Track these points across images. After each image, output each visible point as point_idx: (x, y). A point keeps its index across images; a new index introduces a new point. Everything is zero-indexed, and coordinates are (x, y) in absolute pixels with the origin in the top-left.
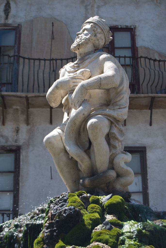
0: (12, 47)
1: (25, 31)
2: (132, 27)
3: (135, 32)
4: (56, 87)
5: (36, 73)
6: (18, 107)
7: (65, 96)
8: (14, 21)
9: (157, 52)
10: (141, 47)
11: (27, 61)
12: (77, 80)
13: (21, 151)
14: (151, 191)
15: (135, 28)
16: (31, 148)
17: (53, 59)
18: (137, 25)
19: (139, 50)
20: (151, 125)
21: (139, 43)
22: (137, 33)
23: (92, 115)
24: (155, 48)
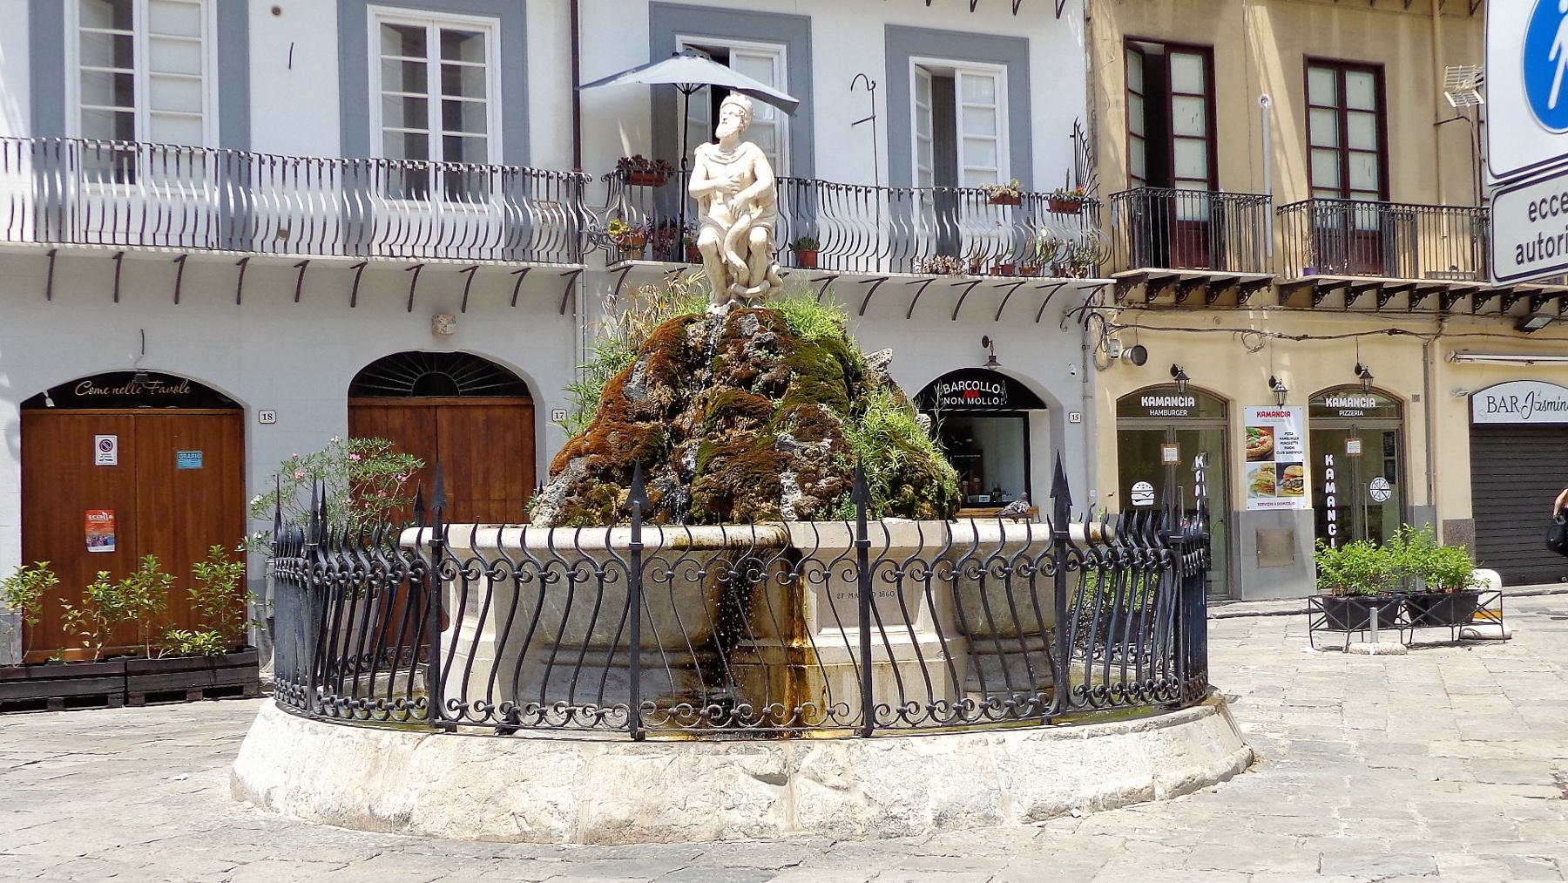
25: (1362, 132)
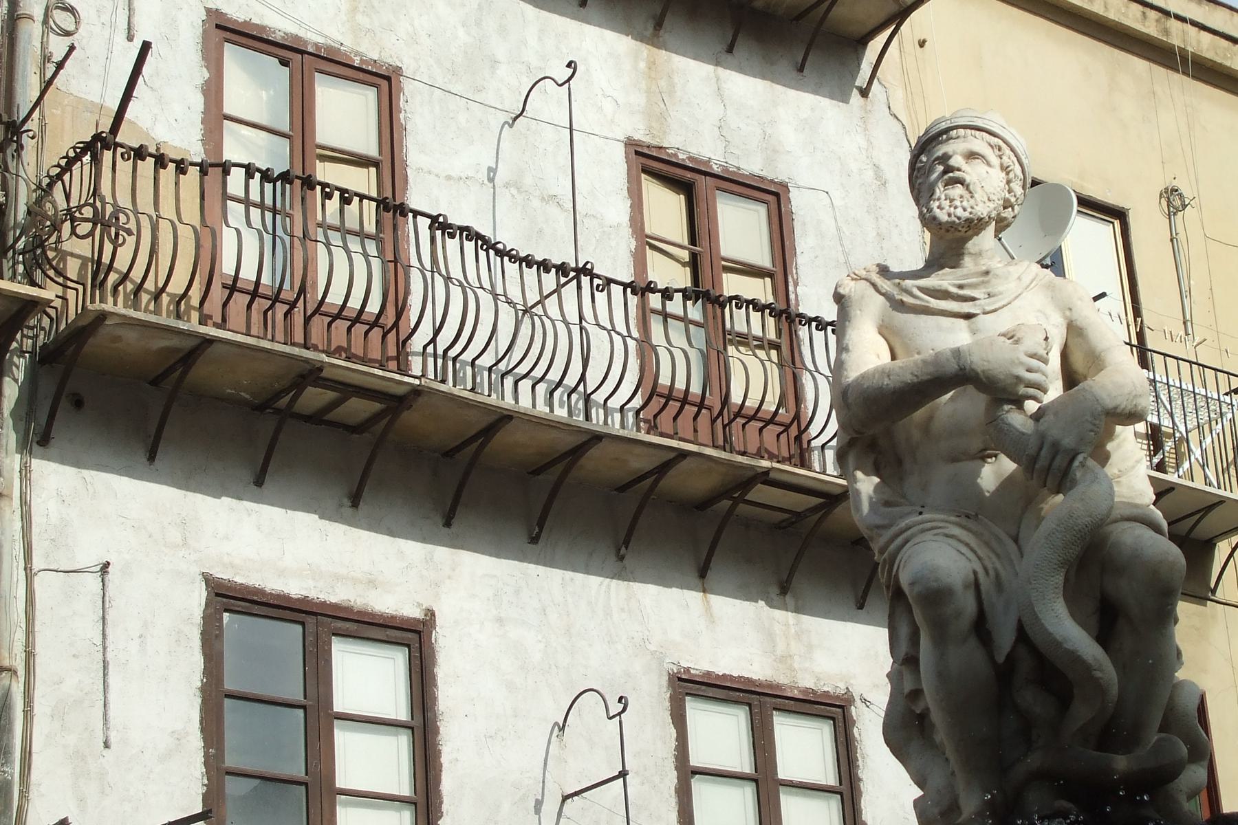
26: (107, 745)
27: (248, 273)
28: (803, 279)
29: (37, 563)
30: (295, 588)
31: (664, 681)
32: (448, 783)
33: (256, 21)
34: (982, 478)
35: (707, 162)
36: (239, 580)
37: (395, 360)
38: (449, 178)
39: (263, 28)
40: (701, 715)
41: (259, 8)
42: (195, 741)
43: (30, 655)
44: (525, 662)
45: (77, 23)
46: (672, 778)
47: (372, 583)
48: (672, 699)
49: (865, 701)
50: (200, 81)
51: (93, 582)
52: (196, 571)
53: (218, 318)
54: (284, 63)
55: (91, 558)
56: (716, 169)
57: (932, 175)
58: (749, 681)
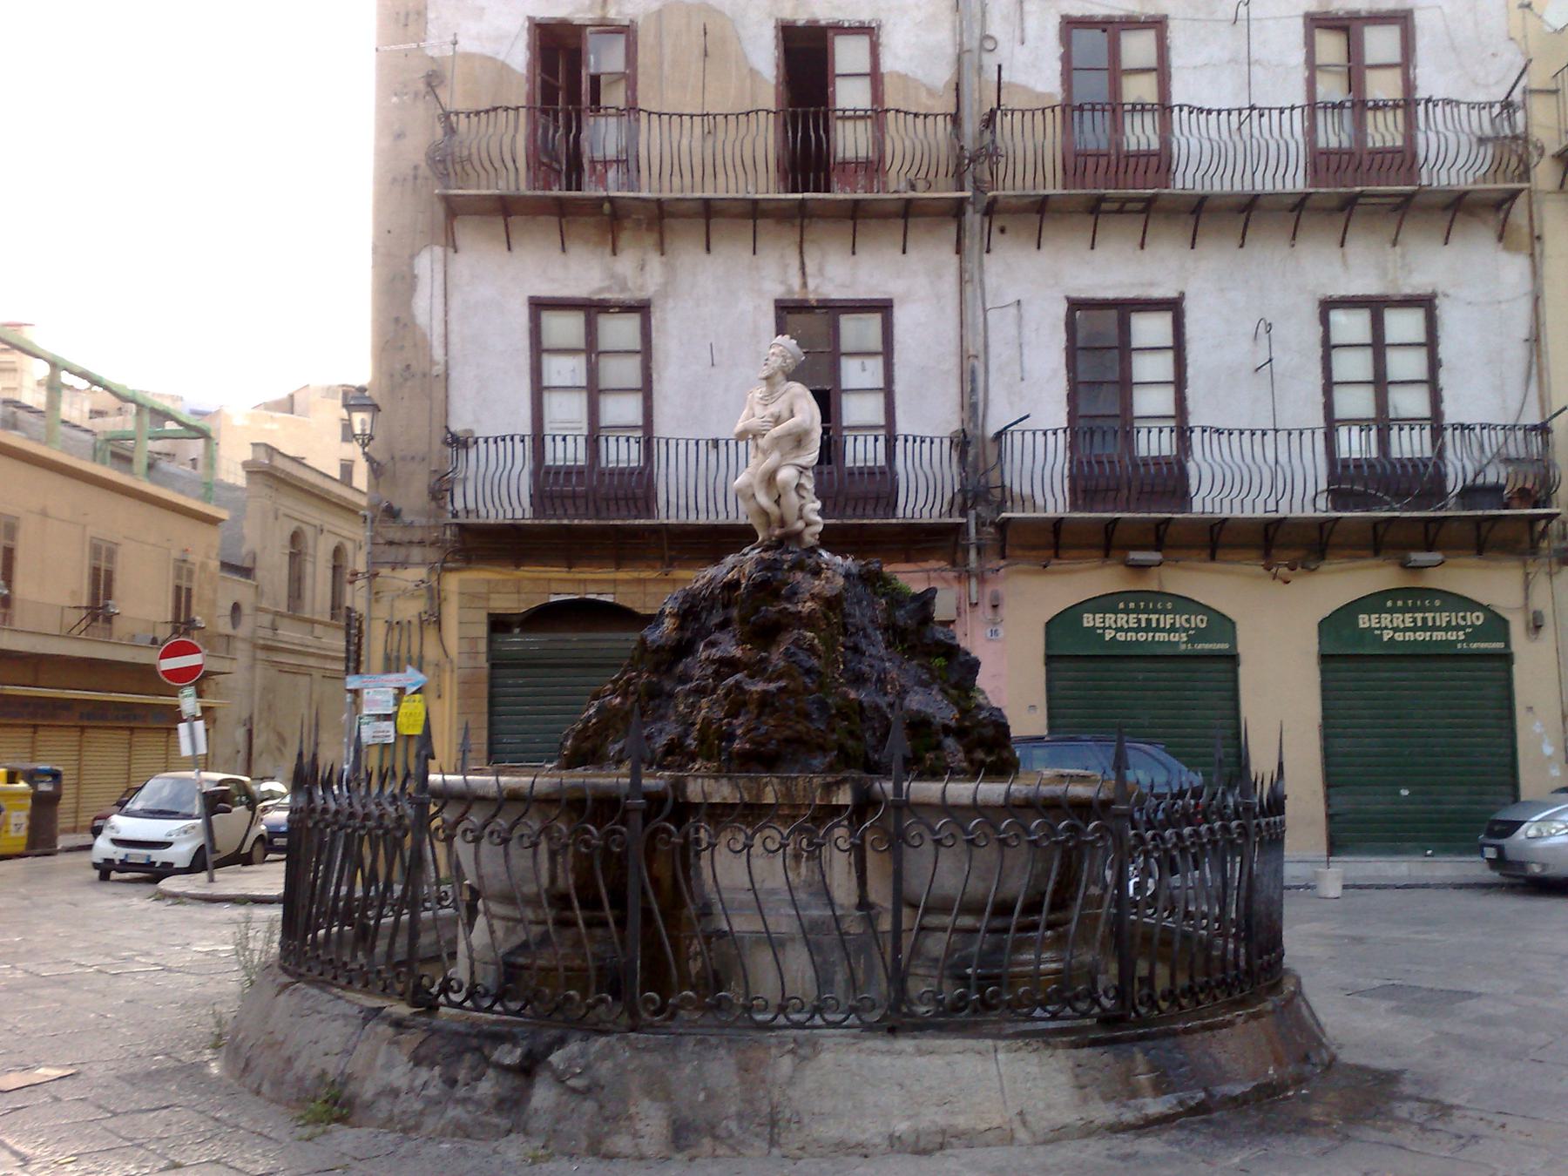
0: (618, 77)
1: (645, 39)
2: (874, 25)
3: (878, 37)
4: (1049, 871)
5: (675, 145)
6: (642, 217)
7: (825, 431)
8: (619, 13)
9: (924, 85)
10: (891, 73)
11: (654, 118)
12: (773, 892)
13: (652, 309)
14: (899, 388)
15: (879, 27)
16: (671, 303)
17: (708, 115)
18: (883, 16)
19: (887, 80)
20: (904, 252)
21: (888, 64)
22: (883, 39)
23: (876, 158)
24: (920, 75)
25: (620, 371)
26: (1022, 379)
27: (1137, 117)
28: (1419, 64)
29: (988, 306)
30: (1110, 294)
31: (1317, 304)
32: (1190, 372)
33: (1087, 13)
34: (982, 692)
35: (1358, 12)
36: (1083, 296)
37: (1319, 66)
38: (1195, 68)
39: (1091, 16)
40: (1338, 317)
41: (1088, 6)
42: (1063, 372)
43: (986, 346)
44: (846, 632)
45: (996, 43)
46: (1319, 352)
47: (1151, 284)
48: (1321, 313)
49: (1446, 295)
50: (1058, 55)
51: (1013, 311)
52: (1063, 295)
53: (632, 440)
54: (1104, 31)
55: (1011, 299)
56: (1363, 14)
57: (680, 567)
58: (1369, 296)
